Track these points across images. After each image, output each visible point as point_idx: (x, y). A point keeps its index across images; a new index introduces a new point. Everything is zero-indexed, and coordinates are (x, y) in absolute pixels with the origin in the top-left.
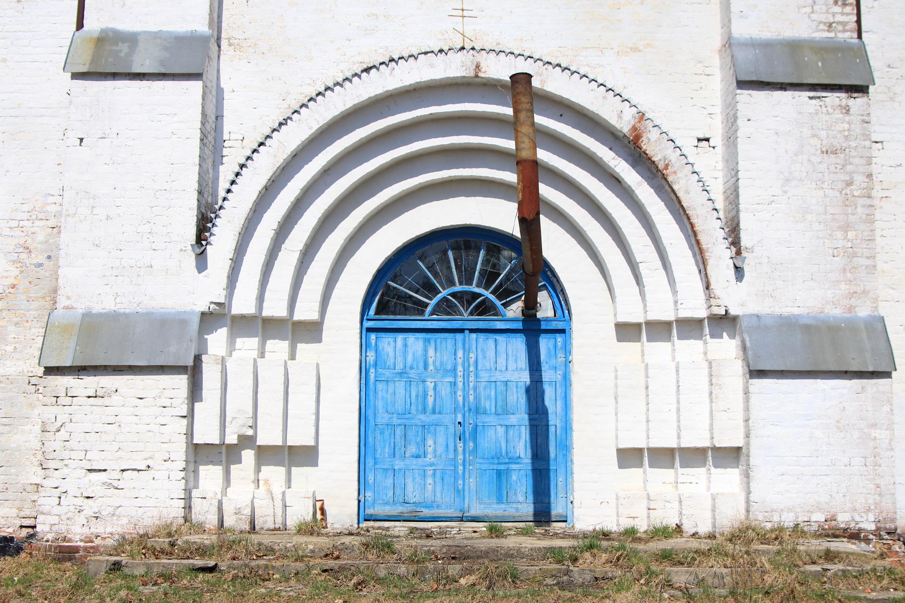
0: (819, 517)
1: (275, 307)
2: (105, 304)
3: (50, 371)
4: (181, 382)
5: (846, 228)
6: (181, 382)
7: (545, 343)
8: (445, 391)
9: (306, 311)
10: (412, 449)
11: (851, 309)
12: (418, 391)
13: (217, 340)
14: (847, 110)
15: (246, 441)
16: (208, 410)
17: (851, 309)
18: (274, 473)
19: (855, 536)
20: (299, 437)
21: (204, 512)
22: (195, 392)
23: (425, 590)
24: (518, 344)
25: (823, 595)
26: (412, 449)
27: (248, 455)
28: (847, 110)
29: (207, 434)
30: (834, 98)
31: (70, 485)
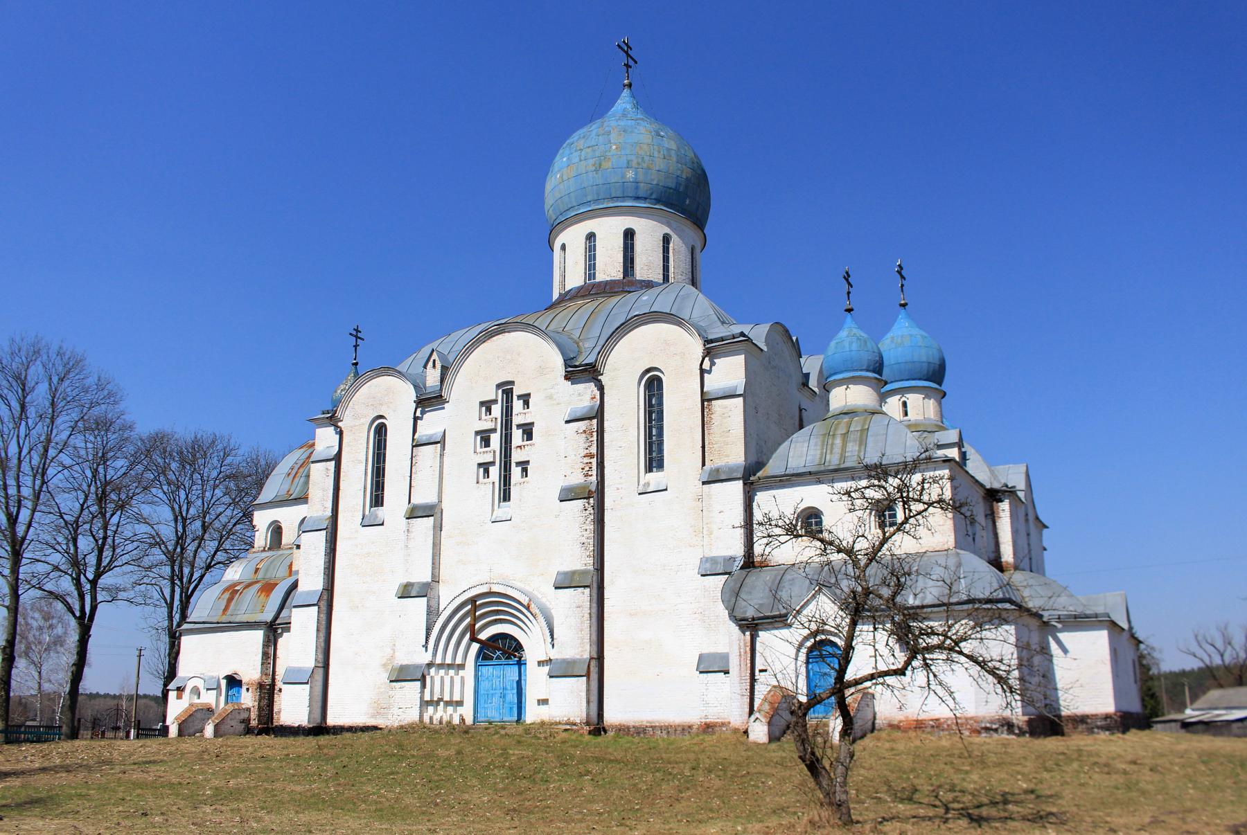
0: (566, 719)
1: (448, 661)
2: (405, 662)
3: (391, 681)
4: (418, 684)
5: (581, 631)
6: (418, 684)
7: (523, 667)
8: (498, 683)
9: (459, 661)
10: (489, 701)
11: (582, 655)
12: (941, 684)
13: (433, 671)
14: (583, 593)
15: (440, 700)
16: (427, 691)
17: (582, 655)
18: (450, 709)
19: (575, 724)
20: (457, 698)
21: (426, 719)
22: (424, 686)
23: (1141, 785)
24: (516, 668)
25: (668, 749)
26: (489, 701)
27: (442, 703)
28: (583, 593)
29: (427, 697)
30: (580, 590)
31: (395, 712)
